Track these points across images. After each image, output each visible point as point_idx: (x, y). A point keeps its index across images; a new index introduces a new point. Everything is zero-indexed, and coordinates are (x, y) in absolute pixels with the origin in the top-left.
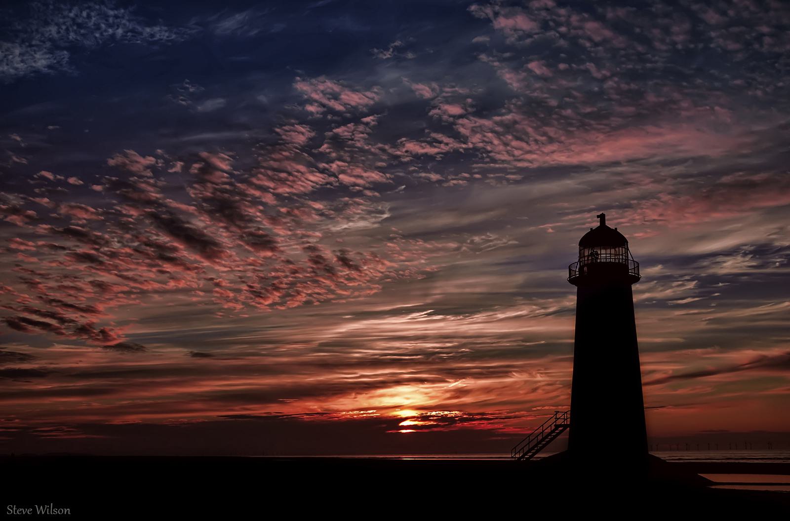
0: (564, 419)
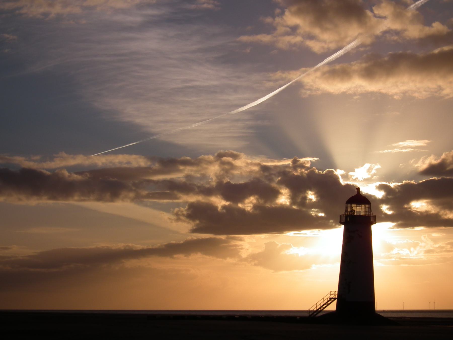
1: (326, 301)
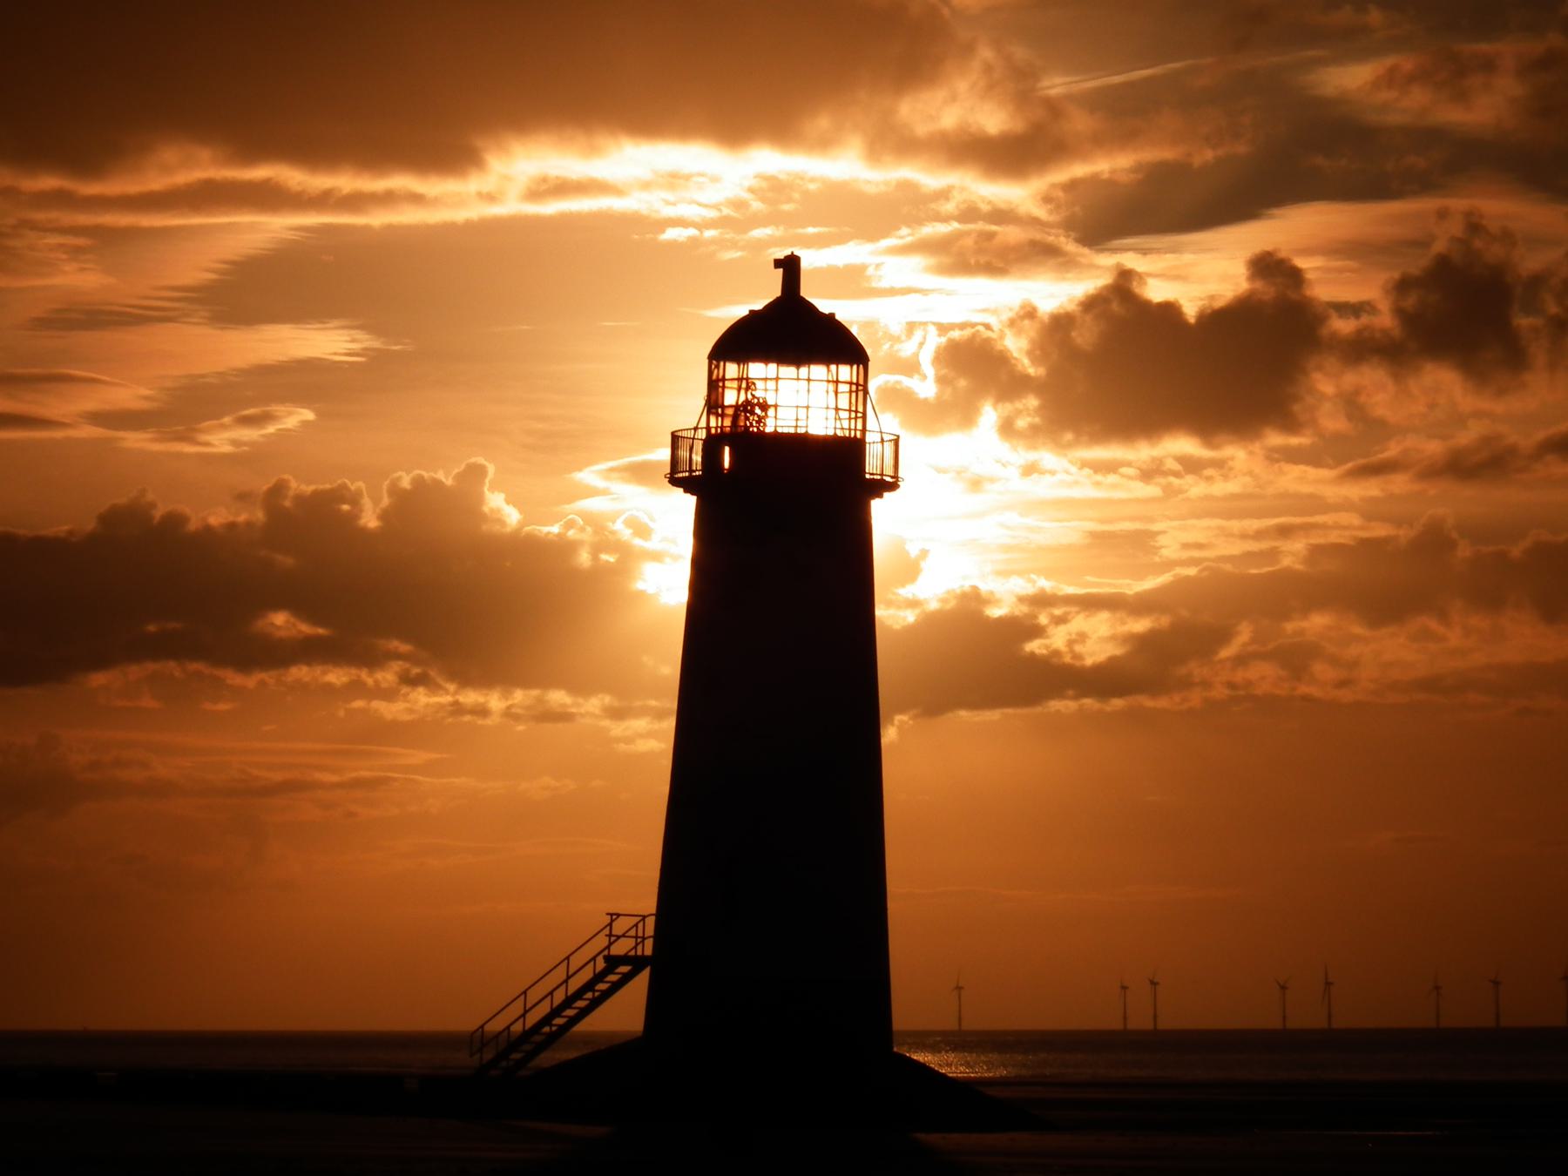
0: (636, 937)
1: (587, 974)
